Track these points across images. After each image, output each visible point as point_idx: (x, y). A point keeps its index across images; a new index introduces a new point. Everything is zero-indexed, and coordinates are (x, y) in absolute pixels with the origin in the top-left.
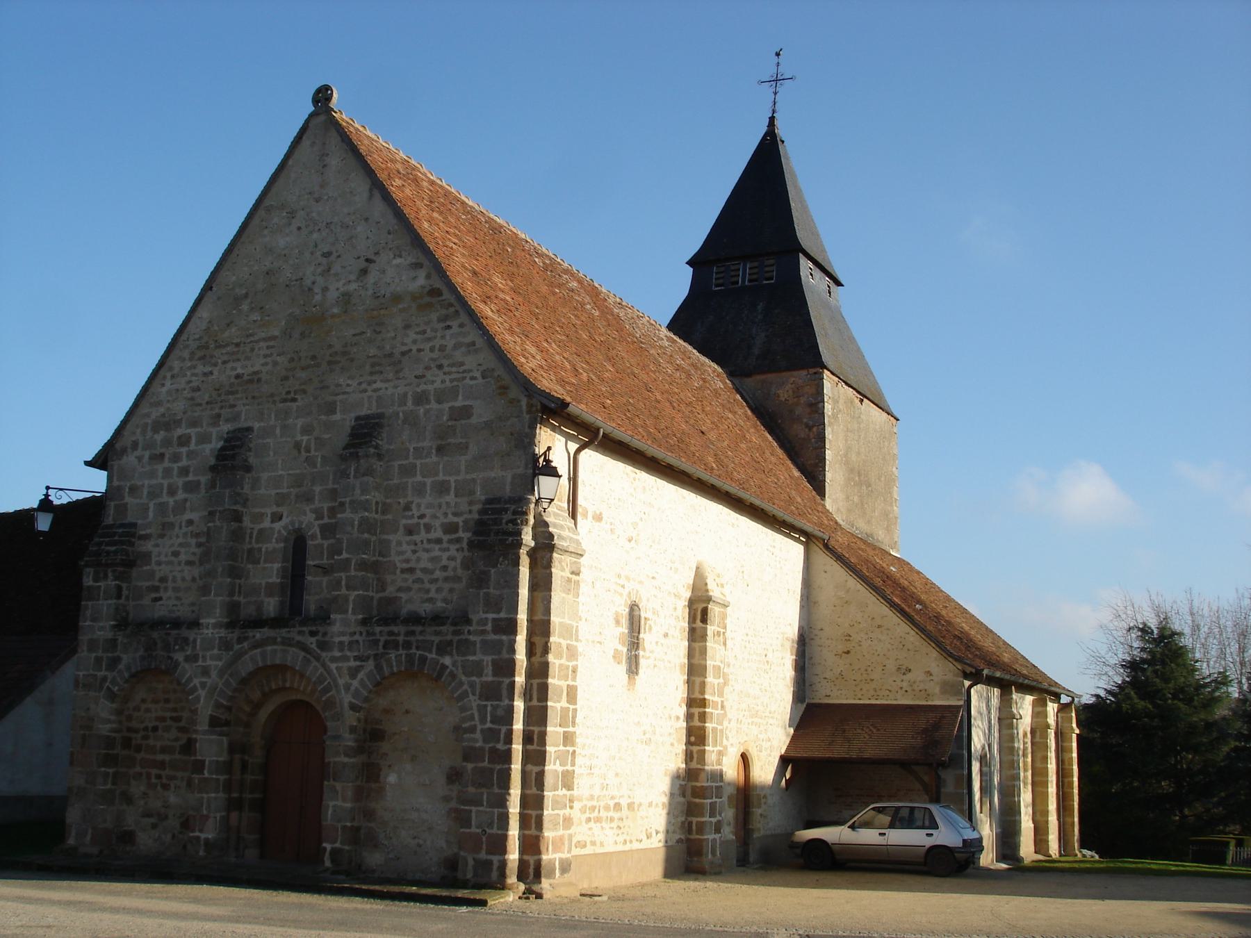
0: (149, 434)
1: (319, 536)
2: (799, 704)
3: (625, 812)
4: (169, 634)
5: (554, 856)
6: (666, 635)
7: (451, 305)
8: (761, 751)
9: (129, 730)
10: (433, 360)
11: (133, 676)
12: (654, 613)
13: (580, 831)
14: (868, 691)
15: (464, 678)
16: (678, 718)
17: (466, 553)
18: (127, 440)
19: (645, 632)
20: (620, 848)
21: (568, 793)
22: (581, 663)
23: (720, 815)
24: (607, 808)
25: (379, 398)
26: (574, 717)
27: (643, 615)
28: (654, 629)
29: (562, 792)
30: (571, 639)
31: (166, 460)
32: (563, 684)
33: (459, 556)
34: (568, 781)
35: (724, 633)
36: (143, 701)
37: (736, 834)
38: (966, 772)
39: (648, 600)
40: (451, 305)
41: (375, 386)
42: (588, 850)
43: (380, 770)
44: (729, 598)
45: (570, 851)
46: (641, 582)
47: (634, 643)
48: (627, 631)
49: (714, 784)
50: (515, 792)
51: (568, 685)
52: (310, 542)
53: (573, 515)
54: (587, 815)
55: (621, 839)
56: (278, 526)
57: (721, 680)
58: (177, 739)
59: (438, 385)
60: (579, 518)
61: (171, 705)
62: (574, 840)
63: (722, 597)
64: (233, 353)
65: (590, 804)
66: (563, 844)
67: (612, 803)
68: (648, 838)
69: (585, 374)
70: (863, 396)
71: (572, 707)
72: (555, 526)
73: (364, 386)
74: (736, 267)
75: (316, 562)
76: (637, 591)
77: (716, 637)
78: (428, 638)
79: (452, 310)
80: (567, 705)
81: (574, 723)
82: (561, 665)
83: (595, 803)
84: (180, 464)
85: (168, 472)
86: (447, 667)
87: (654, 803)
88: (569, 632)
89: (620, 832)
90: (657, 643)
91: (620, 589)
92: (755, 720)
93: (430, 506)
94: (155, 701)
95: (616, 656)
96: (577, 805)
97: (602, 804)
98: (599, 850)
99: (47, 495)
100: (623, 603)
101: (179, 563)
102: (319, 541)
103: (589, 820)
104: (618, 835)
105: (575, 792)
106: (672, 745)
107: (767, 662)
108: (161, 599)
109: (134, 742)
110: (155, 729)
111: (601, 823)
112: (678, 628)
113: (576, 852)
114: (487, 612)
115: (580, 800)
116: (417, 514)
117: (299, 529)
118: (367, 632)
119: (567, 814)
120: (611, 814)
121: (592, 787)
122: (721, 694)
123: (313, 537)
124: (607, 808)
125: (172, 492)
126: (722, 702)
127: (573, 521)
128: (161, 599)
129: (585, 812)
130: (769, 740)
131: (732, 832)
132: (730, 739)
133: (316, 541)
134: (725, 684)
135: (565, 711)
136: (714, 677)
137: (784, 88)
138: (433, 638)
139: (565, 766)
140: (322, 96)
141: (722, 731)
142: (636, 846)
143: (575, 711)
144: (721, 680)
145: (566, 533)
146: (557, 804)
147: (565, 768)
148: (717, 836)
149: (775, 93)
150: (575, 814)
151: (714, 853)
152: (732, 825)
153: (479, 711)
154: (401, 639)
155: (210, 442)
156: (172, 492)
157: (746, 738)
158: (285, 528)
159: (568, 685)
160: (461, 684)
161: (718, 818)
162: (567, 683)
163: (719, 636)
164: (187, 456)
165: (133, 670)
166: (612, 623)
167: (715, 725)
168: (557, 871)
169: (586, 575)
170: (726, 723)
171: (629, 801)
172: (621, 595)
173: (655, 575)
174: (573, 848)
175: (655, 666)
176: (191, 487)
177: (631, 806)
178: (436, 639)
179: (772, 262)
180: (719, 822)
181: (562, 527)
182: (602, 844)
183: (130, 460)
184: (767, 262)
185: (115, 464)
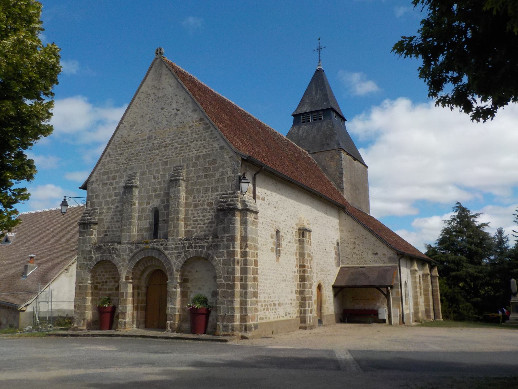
0: (102, 177)
1: (163, 210)
2: (338, 267)
3: (277, 307)
4: (110, 247)
5: (252, 323)
6: (290, 242)
7: (208, 124)
8: (325, 284)
9: (97, 283)
10: (202, 144)
11: (98, 263)
12: (285, 234)
13: (261, 314)
14: (362, 262)
15: (216, 258)
16: (295, 272)
17: (216, 213)
18: (93, 179)
19: (282, 241)
20: (276, 319)
21: (256, 299)
22: (259, 252)
23: (312, 307)
24: (270, 305)
25: (183, 159)
26: (257, 271)
27: (281, 235)
28: (285, 240)
29: (254, 299)
30: (255, 243)
31: (108, 185)
32: (253, 259)
33: (213, 214)
34: (256, 295)
35: (310, 241)
36: (102, 272)
37: (317, 314)
38: (400, 290)
39: (283, 229)
40: (208, 124)
41: (181, 155)
42: (264, 321)
43: (188, 293)
44: (311, 229)
45: (257, 321)
46: (280, 223)
47: (278, 245)
48: (275, 240)
49: (309, 296)
50: (237, 300)
51: (255, 260)
52: (160, 212)
53: (254, 197)
54: (263, 308)
55: (276, 316)
56: (148, 206)
57: (310, 258)
58: (114, 285)
59: (204, 153)
60: (257, 200)
61: (112, 273)
62: (259, 317)
63: (309, 228)
64: (131, 146)
65: (264, 304)
66: (255, 318)
67: (272, 303)
68: (286, 316)
69: (257, 149)
70: (355, 159)
71: (256, 268)
72: (248, 202)
73: (177, 155)
74: (309, 115)
75: (163, 219)
76: (279, 226)
77: (308, 243)
78: (203, 244)
79: (208, 126)
80: (255, 267)
81: (257, 274)
82: (252, 252)
83: (266, 303)
84: (113, 186)
85: (109, 189)
86: (211, 254)
87: (288, 303)
88: (254, 240)
89: (275, 314)
90: (286, 245)
91: (272, 225)
92: (323, 273)
93: (202, 197)
94: (106, 272)
95: (272, 249)
96: (259, 304)
97: (269, 303)
98: (268, 321)
99: (65, 200)
100: (274, 230)
101: (114, 222)
102: (163, 211)
103: (264, 310)
104: (275, 315)
105: (259, 299)
106: (293, 282)
107: (326, 252)
108: (107, 235)
109: (99, 287)
110: (106, 282)
111: (268, 310)
112: (294, 239)
113: (260, 321)
114: (224, 234)
115: (261, 302)
116: (198, 200)
117: (156, 208)
118: (181, 243)
119: (256, 307)
120: (272, 307)
121: (265, 298)
122: (310, 263)
123: (161, 210)
124: (270, 305)
125: (110, 197)
126: (311, 266)
127: (254, 200)
128: (107, 235)
129: (263, 307)
130: (328, 280)
131: (316, 313)
132: (314, 279)
133: (162, 212)
134: (312, 259)
135: (254, 269)
136: (308, 257)
137: (323, 51)
138: (205, 244)
139: (254, 289)
140: (159, 52)
141: (311, 276)
142: (282, 319)
143: (258, 269)
144: (310, 258)
145: (251, 204)
146: (252, 303)
147: (255, 290)
148: (311, 315)
149: (319, 54)
150: (259, 307)
151: (310, 321)
152: (316, 311)
153: (222, 270)
154: (193, 245)
155: (124, 178)
156: (110, 197)
157: (320, 279)
158: (151, 207)
159: (255, 260)
160: (216, 260)
161: (311, 308)
162: (255, 259)
163: (309, 242)
164: (116, 183)
165: (98, 261)
166: (270, 237)
167: (308, 274)
168: (253, 328)
169: (260, 220)
170: (312, 274)
171: (279, 302)
172: (273, 227)
173: (285, 220)
174: (259, 320)
175: (286, 253)
176: (116, 195)
177: (279, 304)
178: (206, 244)
179: (321, 113)
180: (311, 310)
181: (250, 203)
182: (269, 318)
183: (94, 185)
184: (319, 113)
185: (90, 188)
